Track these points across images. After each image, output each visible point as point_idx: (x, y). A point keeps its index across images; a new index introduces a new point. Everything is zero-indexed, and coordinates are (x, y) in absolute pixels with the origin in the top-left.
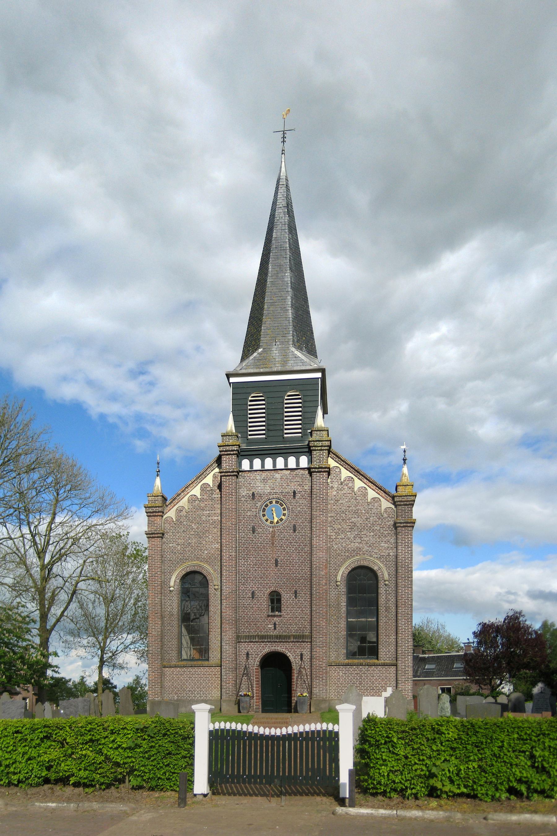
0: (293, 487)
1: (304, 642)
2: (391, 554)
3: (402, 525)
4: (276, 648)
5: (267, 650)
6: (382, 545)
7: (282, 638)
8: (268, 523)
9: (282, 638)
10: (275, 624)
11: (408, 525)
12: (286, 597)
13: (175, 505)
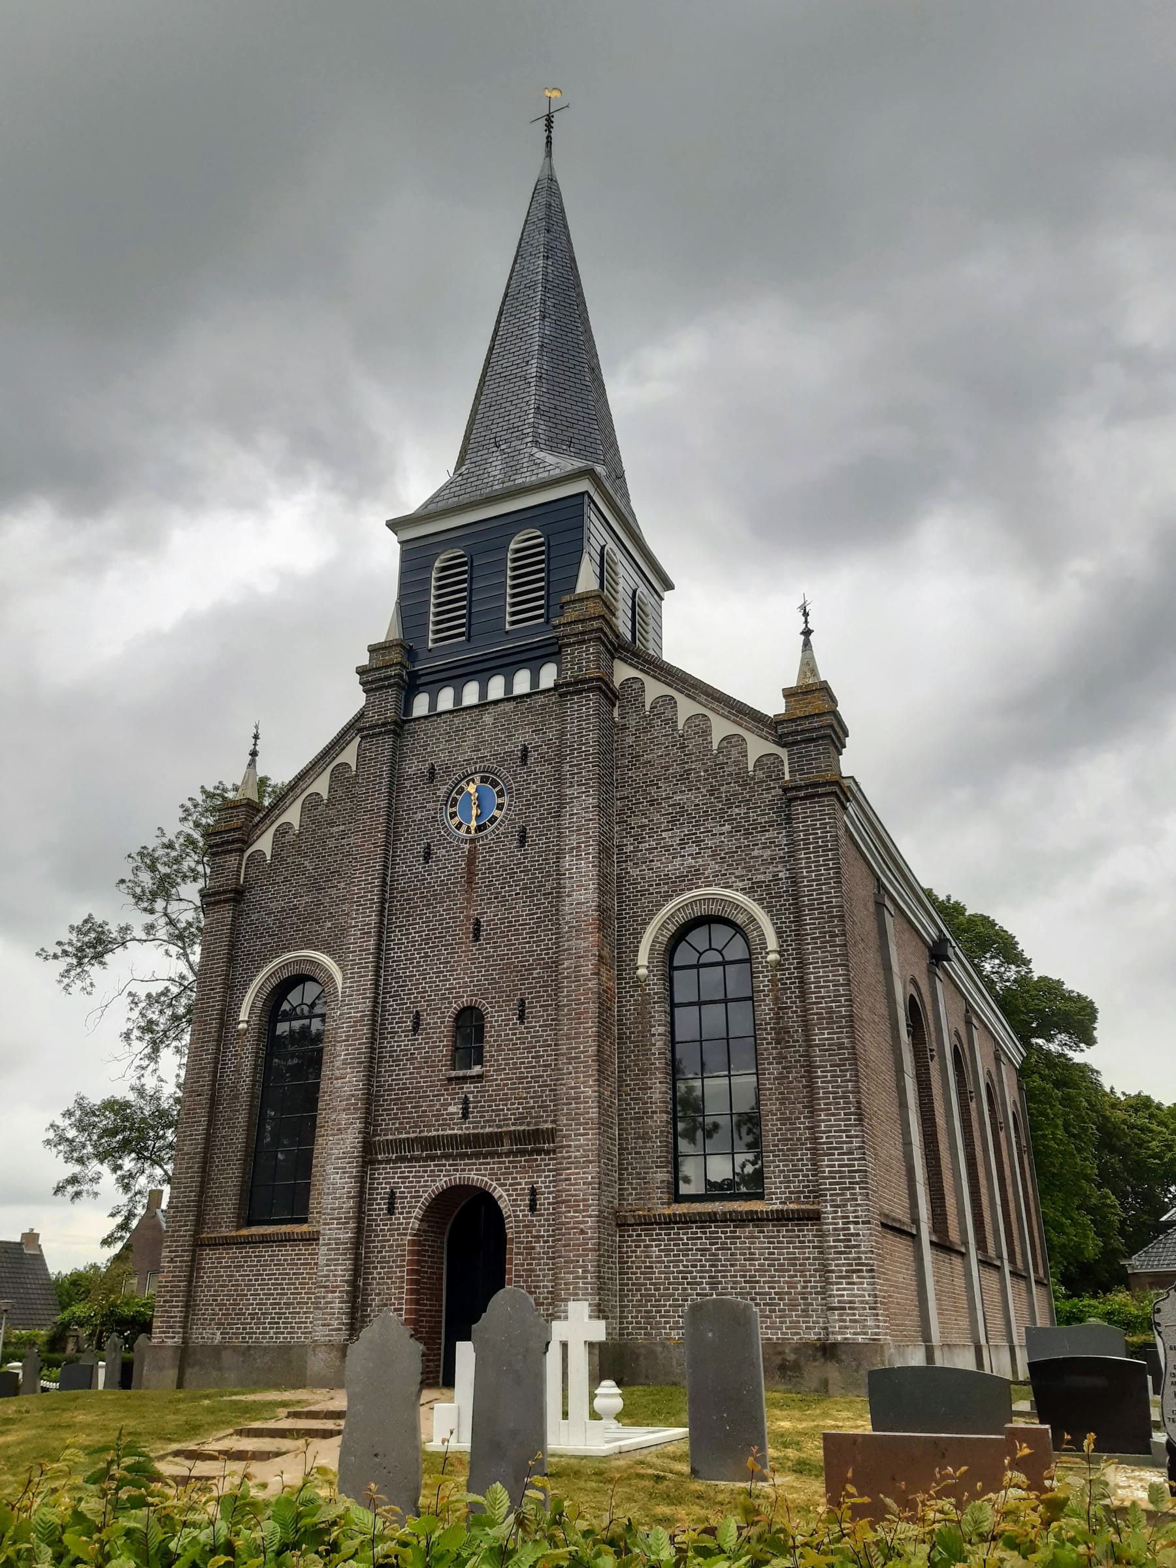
0: (525, 736)
1: (539, 1152)
2: (781, 875)
3: (802, 794)
4: (465, 1175)
5: (442, 1182)
6: (755, 853)
7: (480, 1146)
8: (462, 832)
9: (480, 1146)
10: (466, 1101)
11: (820, 790)
12: (498, 1020)
13: (272, 823)
